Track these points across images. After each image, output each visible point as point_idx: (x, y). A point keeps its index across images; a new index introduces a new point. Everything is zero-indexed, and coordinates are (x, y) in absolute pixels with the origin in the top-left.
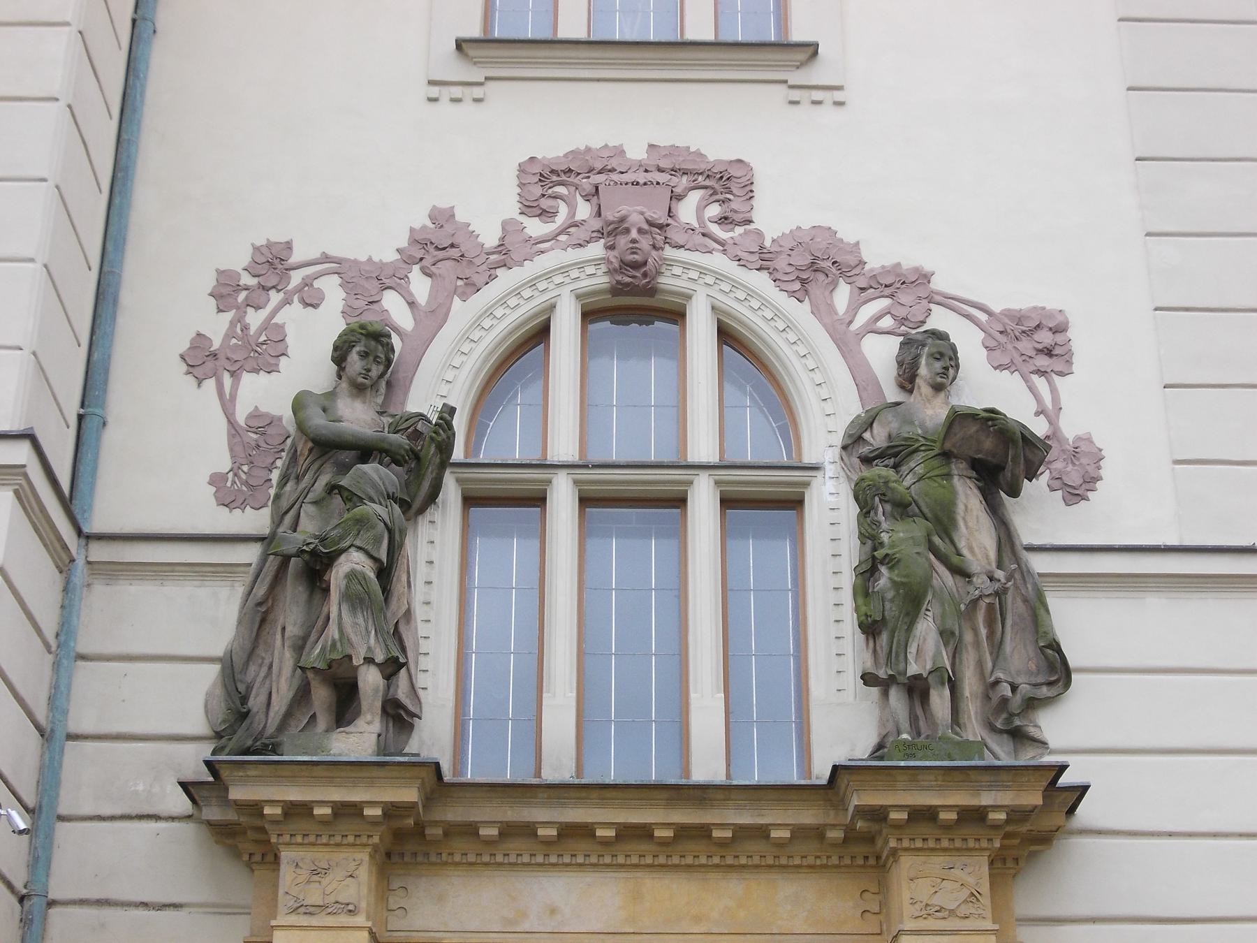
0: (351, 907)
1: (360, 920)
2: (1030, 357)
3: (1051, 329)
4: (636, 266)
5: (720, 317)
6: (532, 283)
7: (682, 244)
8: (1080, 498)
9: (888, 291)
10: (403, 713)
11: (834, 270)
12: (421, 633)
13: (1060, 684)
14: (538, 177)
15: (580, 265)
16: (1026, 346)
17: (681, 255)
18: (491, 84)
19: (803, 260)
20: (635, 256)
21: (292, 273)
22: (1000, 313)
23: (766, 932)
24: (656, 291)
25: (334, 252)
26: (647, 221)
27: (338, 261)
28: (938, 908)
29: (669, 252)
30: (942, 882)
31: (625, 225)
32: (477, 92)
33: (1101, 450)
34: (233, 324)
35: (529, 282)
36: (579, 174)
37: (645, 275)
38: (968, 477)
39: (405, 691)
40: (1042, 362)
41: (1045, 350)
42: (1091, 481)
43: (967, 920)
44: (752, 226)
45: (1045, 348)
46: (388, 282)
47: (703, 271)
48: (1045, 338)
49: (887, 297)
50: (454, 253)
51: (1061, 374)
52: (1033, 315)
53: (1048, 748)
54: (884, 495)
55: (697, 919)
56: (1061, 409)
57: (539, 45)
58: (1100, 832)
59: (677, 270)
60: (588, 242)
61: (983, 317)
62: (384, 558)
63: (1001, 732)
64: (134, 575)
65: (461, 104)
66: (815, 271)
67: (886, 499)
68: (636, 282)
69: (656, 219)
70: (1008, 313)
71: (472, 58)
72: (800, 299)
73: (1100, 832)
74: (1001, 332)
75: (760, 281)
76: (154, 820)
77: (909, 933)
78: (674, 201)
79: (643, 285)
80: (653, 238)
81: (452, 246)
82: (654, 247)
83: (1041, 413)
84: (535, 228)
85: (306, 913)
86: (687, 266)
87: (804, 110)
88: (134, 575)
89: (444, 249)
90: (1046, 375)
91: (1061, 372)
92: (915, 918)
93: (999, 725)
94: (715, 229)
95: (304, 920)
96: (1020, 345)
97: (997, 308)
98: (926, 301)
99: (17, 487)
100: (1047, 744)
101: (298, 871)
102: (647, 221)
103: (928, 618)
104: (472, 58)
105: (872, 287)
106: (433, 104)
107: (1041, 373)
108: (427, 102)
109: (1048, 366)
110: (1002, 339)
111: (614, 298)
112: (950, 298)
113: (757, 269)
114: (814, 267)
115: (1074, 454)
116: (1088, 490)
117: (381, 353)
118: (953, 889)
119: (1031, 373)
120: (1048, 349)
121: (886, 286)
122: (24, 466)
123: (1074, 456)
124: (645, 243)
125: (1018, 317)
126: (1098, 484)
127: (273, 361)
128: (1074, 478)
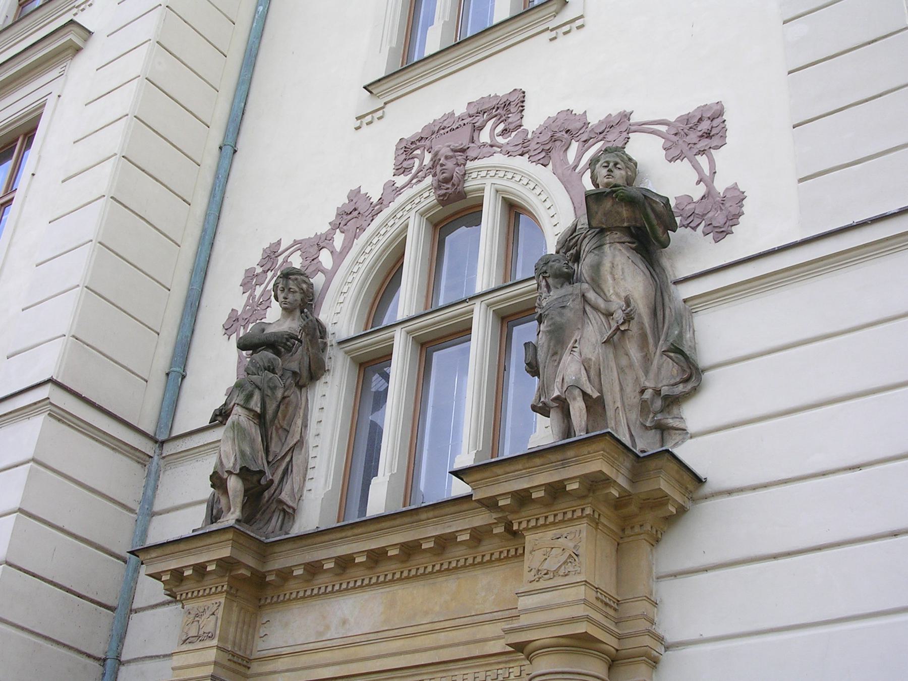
0: (210, 635)
1: (215, 642)
2: (695, 144)
3: (709, 118)
4: (447, 181)
5: (503, 196)
6: (393, 215)
7: (476, 156)
8: (725, 233)
9: (601, 136)
10: (285, 507)
11: (566, 136)
12: (312, 454)
13: (694, 378)
14: (404, 149)
15: (420, 194)
16: (693, 137)
17: (477, 163)
18: (388, 106)
19: (546, 137)
20: (444, 175)
21: (279, 258)
22: (675, 121)
23: (468, 615)
24: (465, 194)
25: (299, 238)
26: (452, 150)
27: (300, 242)
28: (545, 571)
29: (470, 165)
30: (551, 550)
31: (439, 157)
32: (380, 113)
33: (743, 193)
34: (249, 299)
35: (392, 215)
36: (427, 138)
37: (453, 185)
38: (618, 242)
39: (288, 493)
40: (704, 143)
41: (704, 134)
42: (734, 218)
43: (567, 577)
44: (522, 128)
45: (704, 133)
46: (322, 245)
47: (488, 169)
48: (705, 126)
49: (601, 140)
50: (355, 214)
51: (717, 147)
52: (696, 114)
53: (688, 433)
54: (546, 272)
55: (426, 613)
56: (715, 173)
57: (12, 27)
58: (730, 492)
59: (474, 175)
60: (424, 178)
61: (664, 128)
62: (258, 410)
63: (651, 428)
64: (183, 460)
65: (584, 28)
66: (554, 141)
67: (547, 275)
68: (450, 191)
69: (457, 147)
70: (680, 119)
71: (376, 95)
72: (545, 164)
73: (730, 492)
74: (676, 134)
75: (521, 163)
76: (167, 606)
77: (523, 594)
78: (476, 133)
79: (454, 192)
80: (457, 159)
81: (355, 209)
82: (458, 165)
83: (700, 181)
84: (401, 180)
85: (190, 643)
86: (479, 169)
87: (561, 39)
88: (183, 460)
89: (351, 213)
90: (706, 152)
91: (716, 146)
92: (530, 582)
93: (648, 424)
94: (501, 140)
95: (191, 647)
96: (688, 139)
97: (672, 119)
98: (625, 133)
99: (48, 412)
100: (685, 430)
101: (189, 616)
102: (452, 150)
103: (574, 353)
104: (376, 95)
105: (591, 138)
106: (358, 130)
107: (702, 152)
108: (356, 131)
109: (706, 145)
110: (675, 138)
111: (445, 207)
112: (642, 125)
113: (519, 155)
114: (553, 139)
115: (722, 202)
116: (732, 226)
117: (293, 285)
118: (557, 555)
119: (695, 155)
120: (706, 133)
121: (600, 133)
122: (48, 398)
123: (722, 204)
124: (450, 164)
125: (686, 119)
126: (741, 219)
127: (263, 312)
128: (719, 219)
